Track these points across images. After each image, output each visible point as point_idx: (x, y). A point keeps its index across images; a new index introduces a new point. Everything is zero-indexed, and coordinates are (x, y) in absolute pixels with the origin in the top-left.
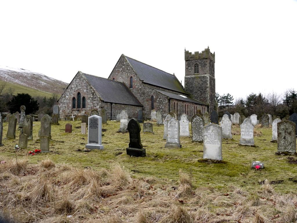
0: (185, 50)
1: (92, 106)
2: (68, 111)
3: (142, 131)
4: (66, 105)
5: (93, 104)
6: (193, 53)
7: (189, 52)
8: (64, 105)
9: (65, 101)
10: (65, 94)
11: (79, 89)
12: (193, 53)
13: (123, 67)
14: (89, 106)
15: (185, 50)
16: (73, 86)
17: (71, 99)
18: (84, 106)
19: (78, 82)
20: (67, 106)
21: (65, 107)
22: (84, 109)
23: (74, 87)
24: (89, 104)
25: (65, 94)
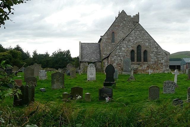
1: (156, 60)
5: (158, 58)
9: (121, 54)
10: (121, 46)
11: (139, 42)
13: (124, 22)
16: (131, 38)
17: (129, 52)
18: (146, 60)
22: (146, 63)
25: (121, 46)
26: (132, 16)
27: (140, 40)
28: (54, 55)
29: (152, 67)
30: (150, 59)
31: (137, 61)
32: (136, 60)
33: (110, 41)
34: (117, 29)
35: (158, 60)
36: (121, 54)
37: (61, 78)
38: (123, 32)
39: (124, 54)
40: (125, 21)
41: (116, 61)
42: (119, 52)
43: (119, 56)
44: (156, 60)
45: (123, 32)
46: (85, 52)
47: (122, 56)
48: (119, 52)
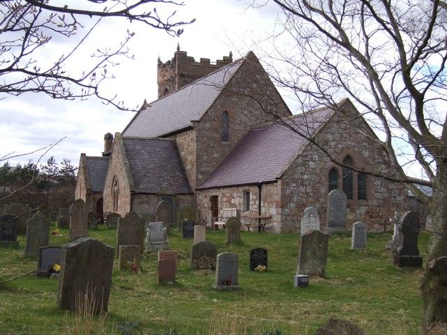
0: (178, 48)
1: (386, 195)
2: (200, 197)
3: (93, 238)
4: (309, 189)
5: (389, 190)
6: (197, 60)
7: (188, 55)
8: (302, 189)
9: (306, 177)
10: (306, 156)
11: (348, 148)
12: (197, 60)
13: (255, 86)
14: (378, 195)
15: (178, 48)
16: (330, 137)
17: (326, 173)
18: (362, 196)
19: (345, 129)
20: (315, 193)
21: (307, 193)
22: (364, 202)
23: (333, 140)
24: (379, 190)
25: (306, 156)
26: (188, 55)
27: (350, 143)
28: (68, 175)
29: (378, 213)
30: (373, 192)
31: (359, 198)
32: (357, 197)
33: (218, 135)
34: (236, 104)
35: (390, 197)
36: (306, 177)
37: (321, 246)
38: (250, 112)
39: (314, 178)
40: (255, 82)
41: (295, 198)
42: (301, 173)
43: (302, 184)
44: (386, 195)
45: (250, 112)
46: (139, 165)
47: (309, 185)
48: (301, 173)
